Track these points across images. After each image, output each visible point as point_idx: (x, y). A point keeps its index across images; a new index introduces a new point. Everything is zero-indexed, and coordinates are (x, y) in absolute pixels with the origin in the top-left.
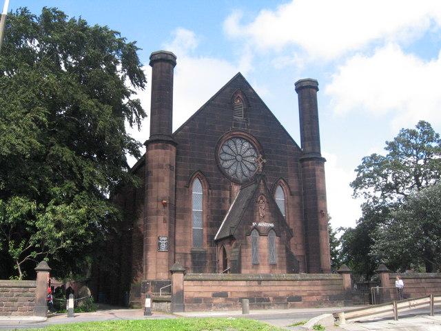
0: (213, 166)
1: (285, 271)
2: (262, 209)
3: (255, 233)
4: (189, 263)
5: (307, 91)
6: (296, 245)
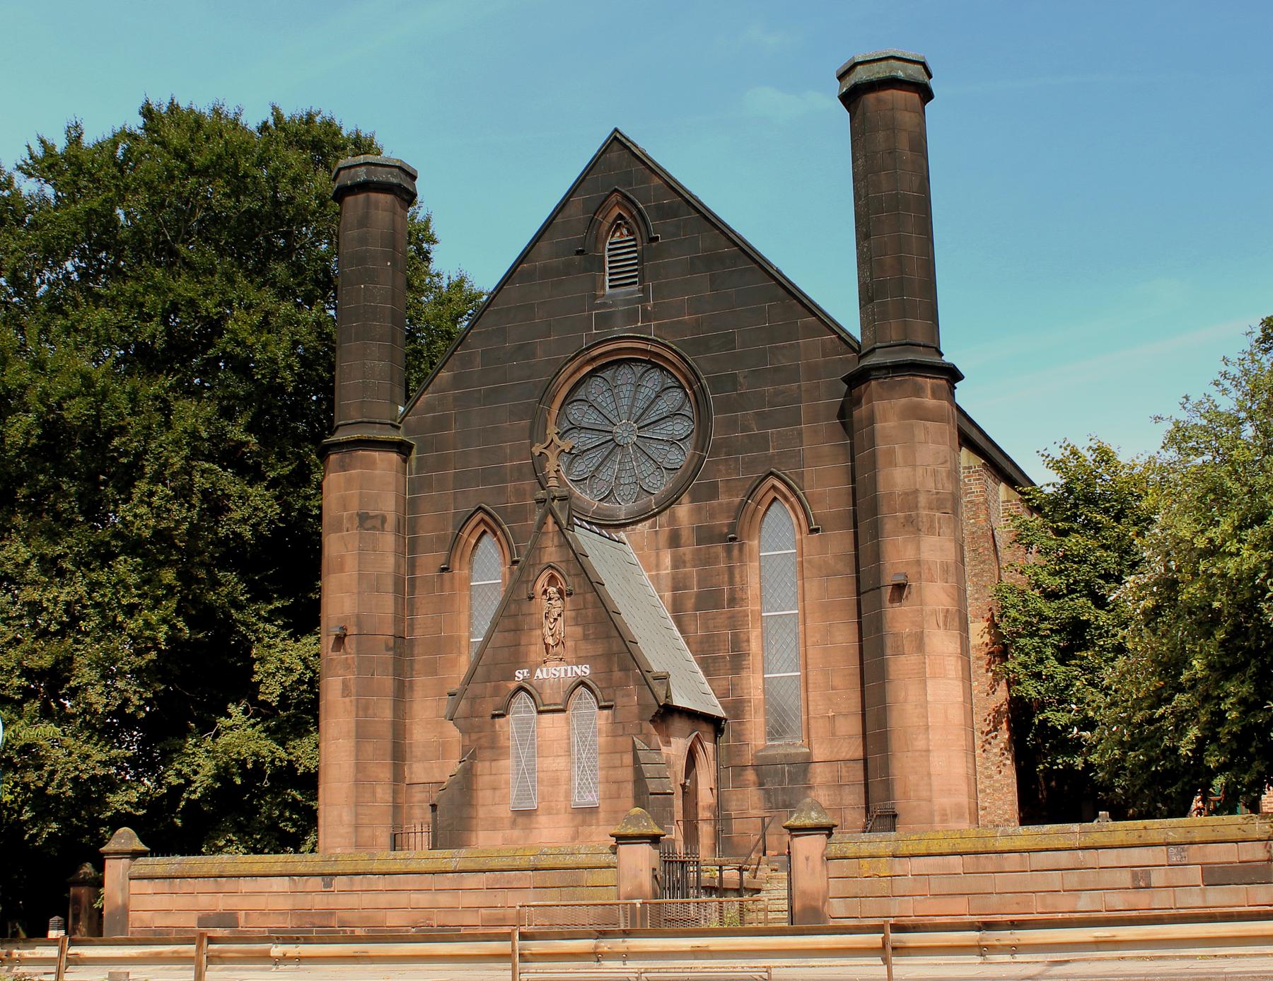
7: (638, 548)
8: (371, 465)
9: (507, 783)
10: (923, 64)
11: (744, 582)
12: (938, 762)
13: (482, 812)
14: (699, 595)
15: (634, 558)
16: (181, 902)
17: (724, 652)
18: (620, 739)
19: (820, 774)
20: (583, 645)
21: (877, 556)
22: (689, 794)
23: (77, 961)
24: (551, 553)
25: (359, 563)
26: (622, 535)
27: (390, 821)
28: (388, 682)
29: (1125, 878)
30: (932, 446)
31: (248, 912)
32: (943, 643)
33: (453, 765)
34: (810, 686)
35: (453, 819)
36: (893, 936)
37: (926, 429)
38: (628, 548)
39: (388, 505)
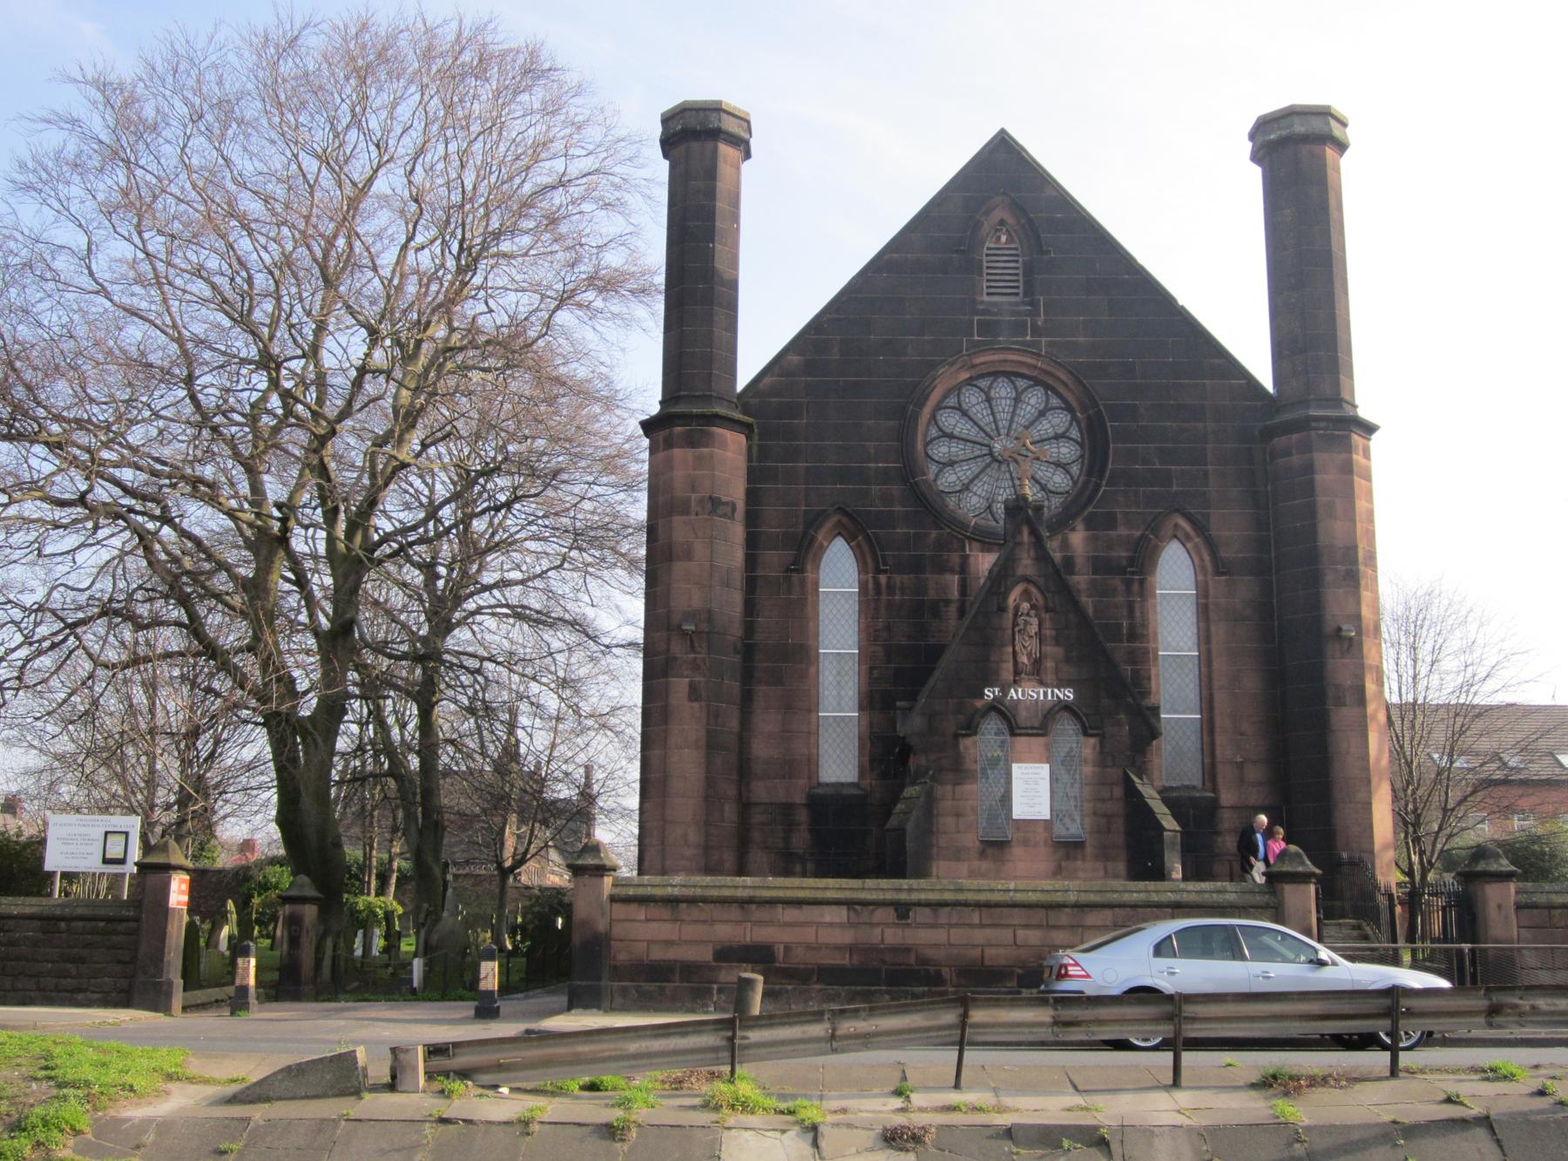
0: (896, 489)
1: (1121, 867)
3: (991, 725)
4: (801, 840)
5: (1296, 158)
6: (1240, 766)
13: (943, 841)
16: (690, 931)
31: (787, 948)
39: (736, 490)
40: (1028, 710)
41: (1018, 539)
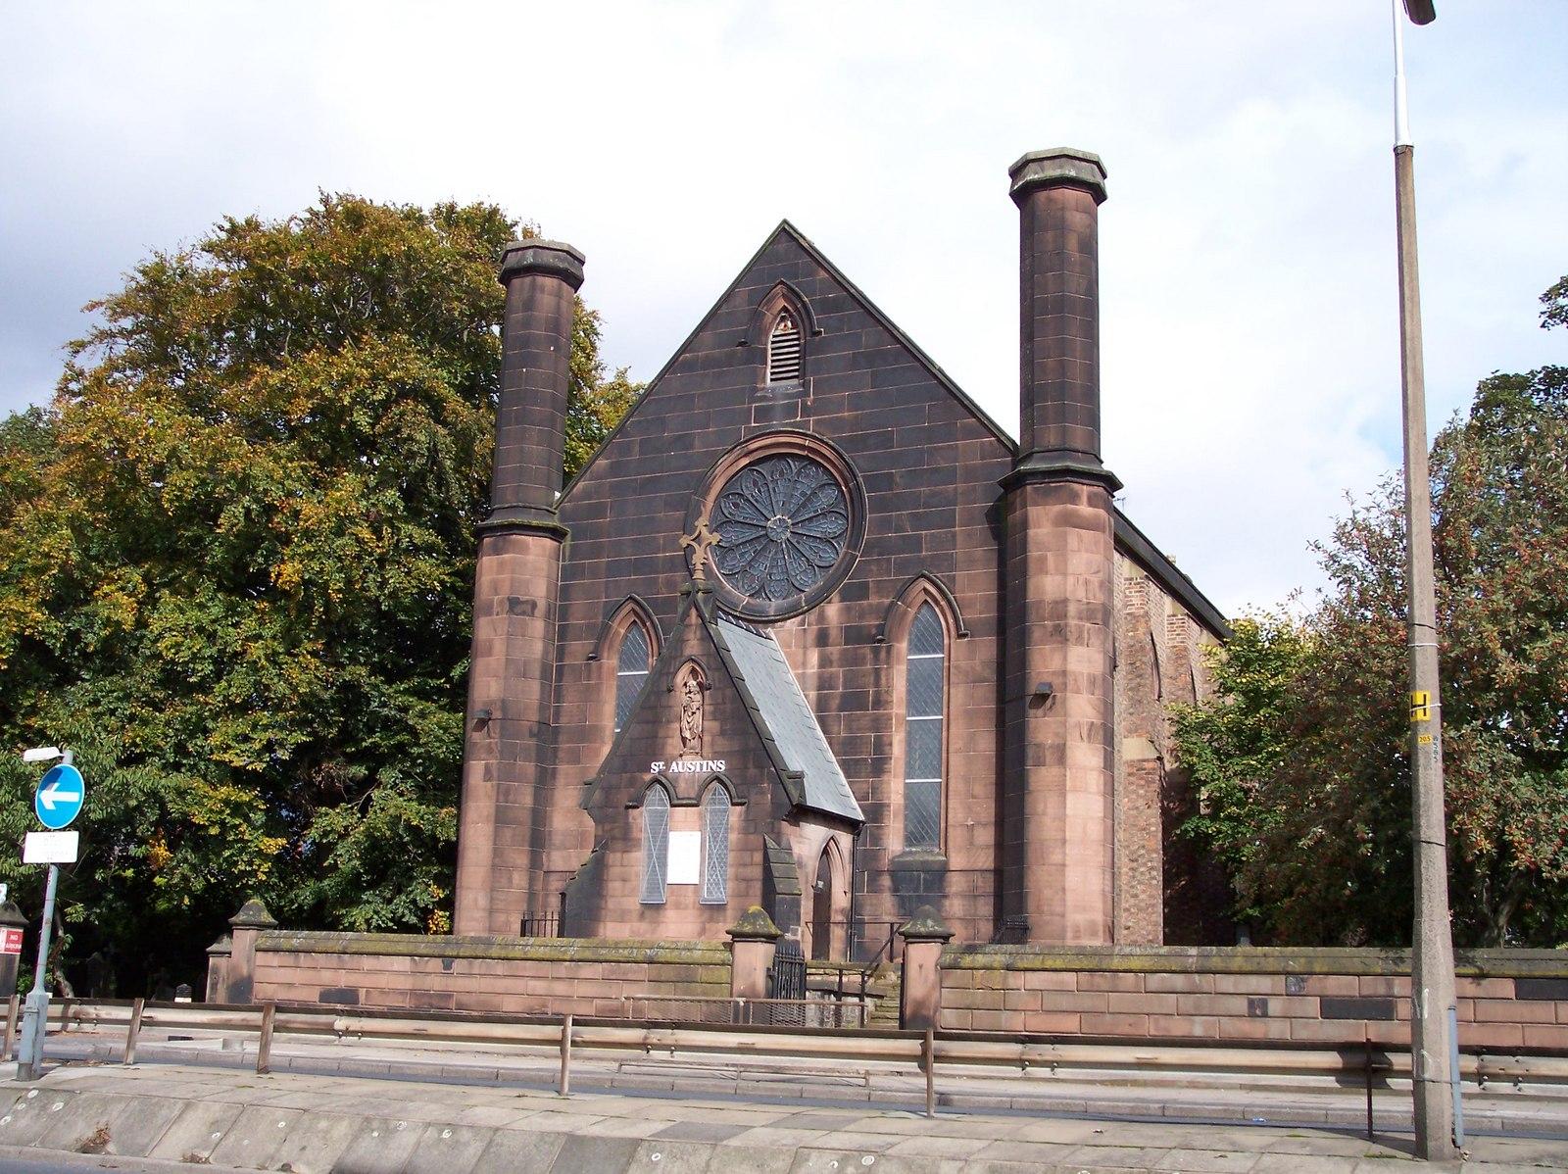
2: (691, 707)
5: (1055, 205)
7: (786, 645)
8: (524, 549)
9: (637, 875)
10: (1098, 164)
11: (889, 686)
12: (1073, 878)
13: (611, 904)
14: (843, 696)
15: (782, 656)
17: (867, 755)
18: (752, 837)
19: (956, 883)
20: (720, 741)
21: (1023, 663)
22: (822, 899)
23: (150, 1023)
24: (693, 646)
25: (508, 647)
26: (770, 631)
27: (525, 907)
28: (529, 768)
29: (1241, 1005)
30: (1085, 556)
32: (1085, 757)
33: (587, 855)
34: (950, 793)
35: (580, 908)
36: (935, 1044)
37: (1080, 537)
38: (775, 644)
39: (539, 590)
40: (687, 780)
41: (687, 622)
